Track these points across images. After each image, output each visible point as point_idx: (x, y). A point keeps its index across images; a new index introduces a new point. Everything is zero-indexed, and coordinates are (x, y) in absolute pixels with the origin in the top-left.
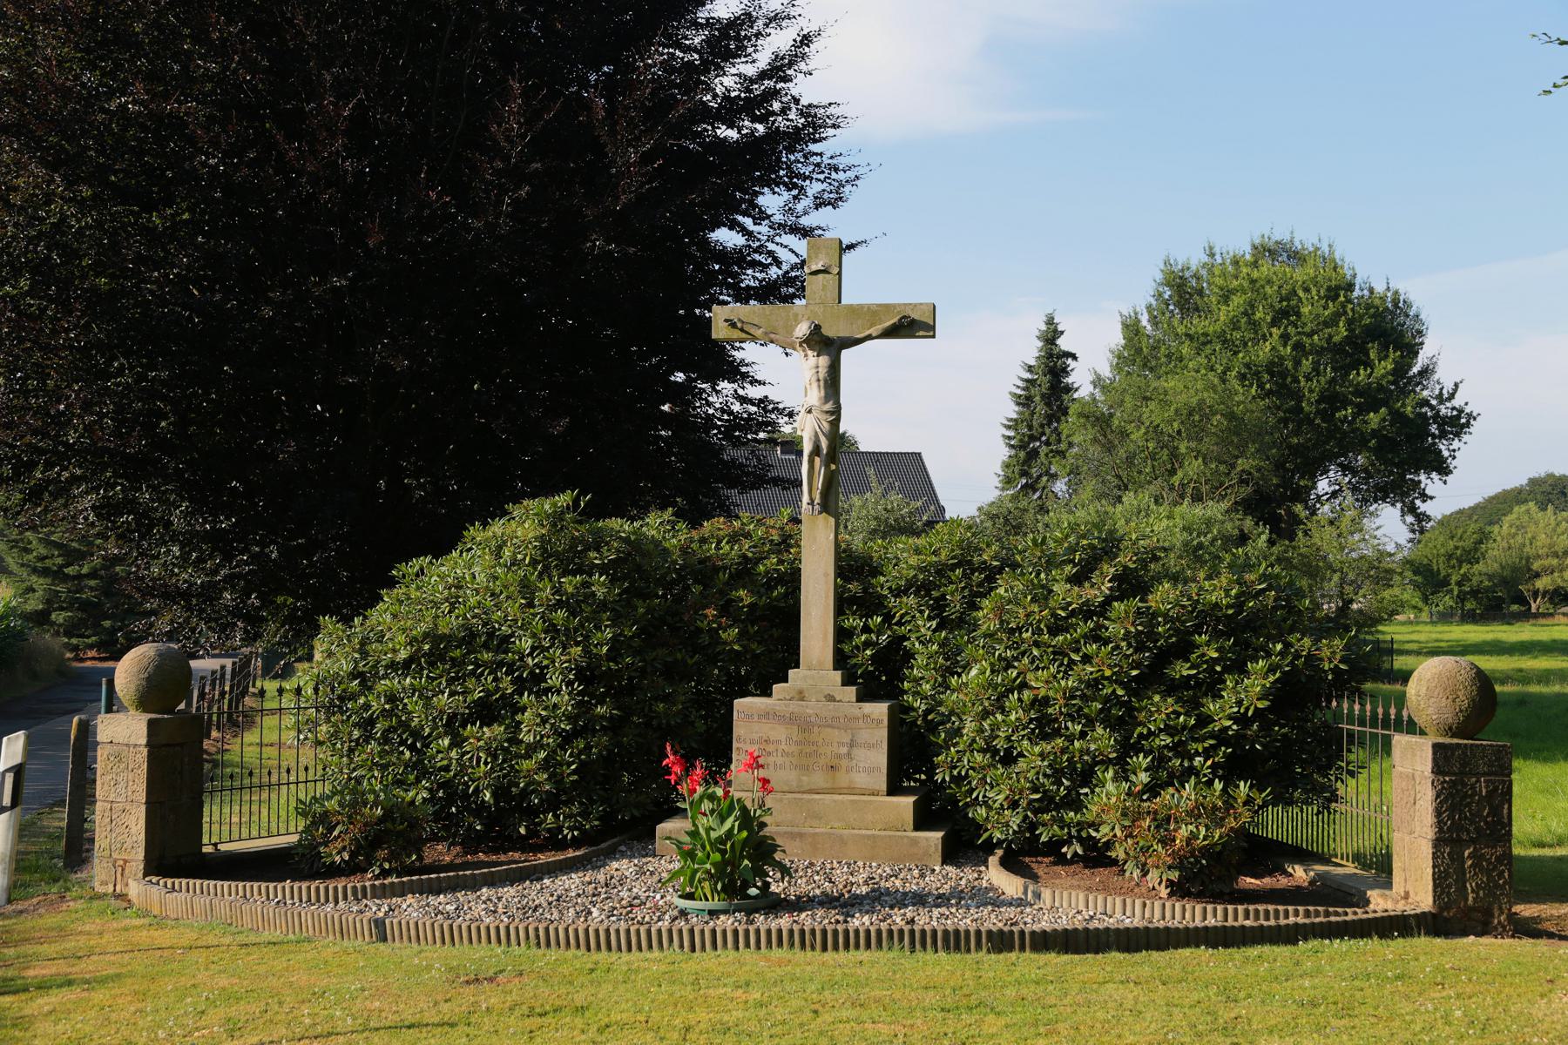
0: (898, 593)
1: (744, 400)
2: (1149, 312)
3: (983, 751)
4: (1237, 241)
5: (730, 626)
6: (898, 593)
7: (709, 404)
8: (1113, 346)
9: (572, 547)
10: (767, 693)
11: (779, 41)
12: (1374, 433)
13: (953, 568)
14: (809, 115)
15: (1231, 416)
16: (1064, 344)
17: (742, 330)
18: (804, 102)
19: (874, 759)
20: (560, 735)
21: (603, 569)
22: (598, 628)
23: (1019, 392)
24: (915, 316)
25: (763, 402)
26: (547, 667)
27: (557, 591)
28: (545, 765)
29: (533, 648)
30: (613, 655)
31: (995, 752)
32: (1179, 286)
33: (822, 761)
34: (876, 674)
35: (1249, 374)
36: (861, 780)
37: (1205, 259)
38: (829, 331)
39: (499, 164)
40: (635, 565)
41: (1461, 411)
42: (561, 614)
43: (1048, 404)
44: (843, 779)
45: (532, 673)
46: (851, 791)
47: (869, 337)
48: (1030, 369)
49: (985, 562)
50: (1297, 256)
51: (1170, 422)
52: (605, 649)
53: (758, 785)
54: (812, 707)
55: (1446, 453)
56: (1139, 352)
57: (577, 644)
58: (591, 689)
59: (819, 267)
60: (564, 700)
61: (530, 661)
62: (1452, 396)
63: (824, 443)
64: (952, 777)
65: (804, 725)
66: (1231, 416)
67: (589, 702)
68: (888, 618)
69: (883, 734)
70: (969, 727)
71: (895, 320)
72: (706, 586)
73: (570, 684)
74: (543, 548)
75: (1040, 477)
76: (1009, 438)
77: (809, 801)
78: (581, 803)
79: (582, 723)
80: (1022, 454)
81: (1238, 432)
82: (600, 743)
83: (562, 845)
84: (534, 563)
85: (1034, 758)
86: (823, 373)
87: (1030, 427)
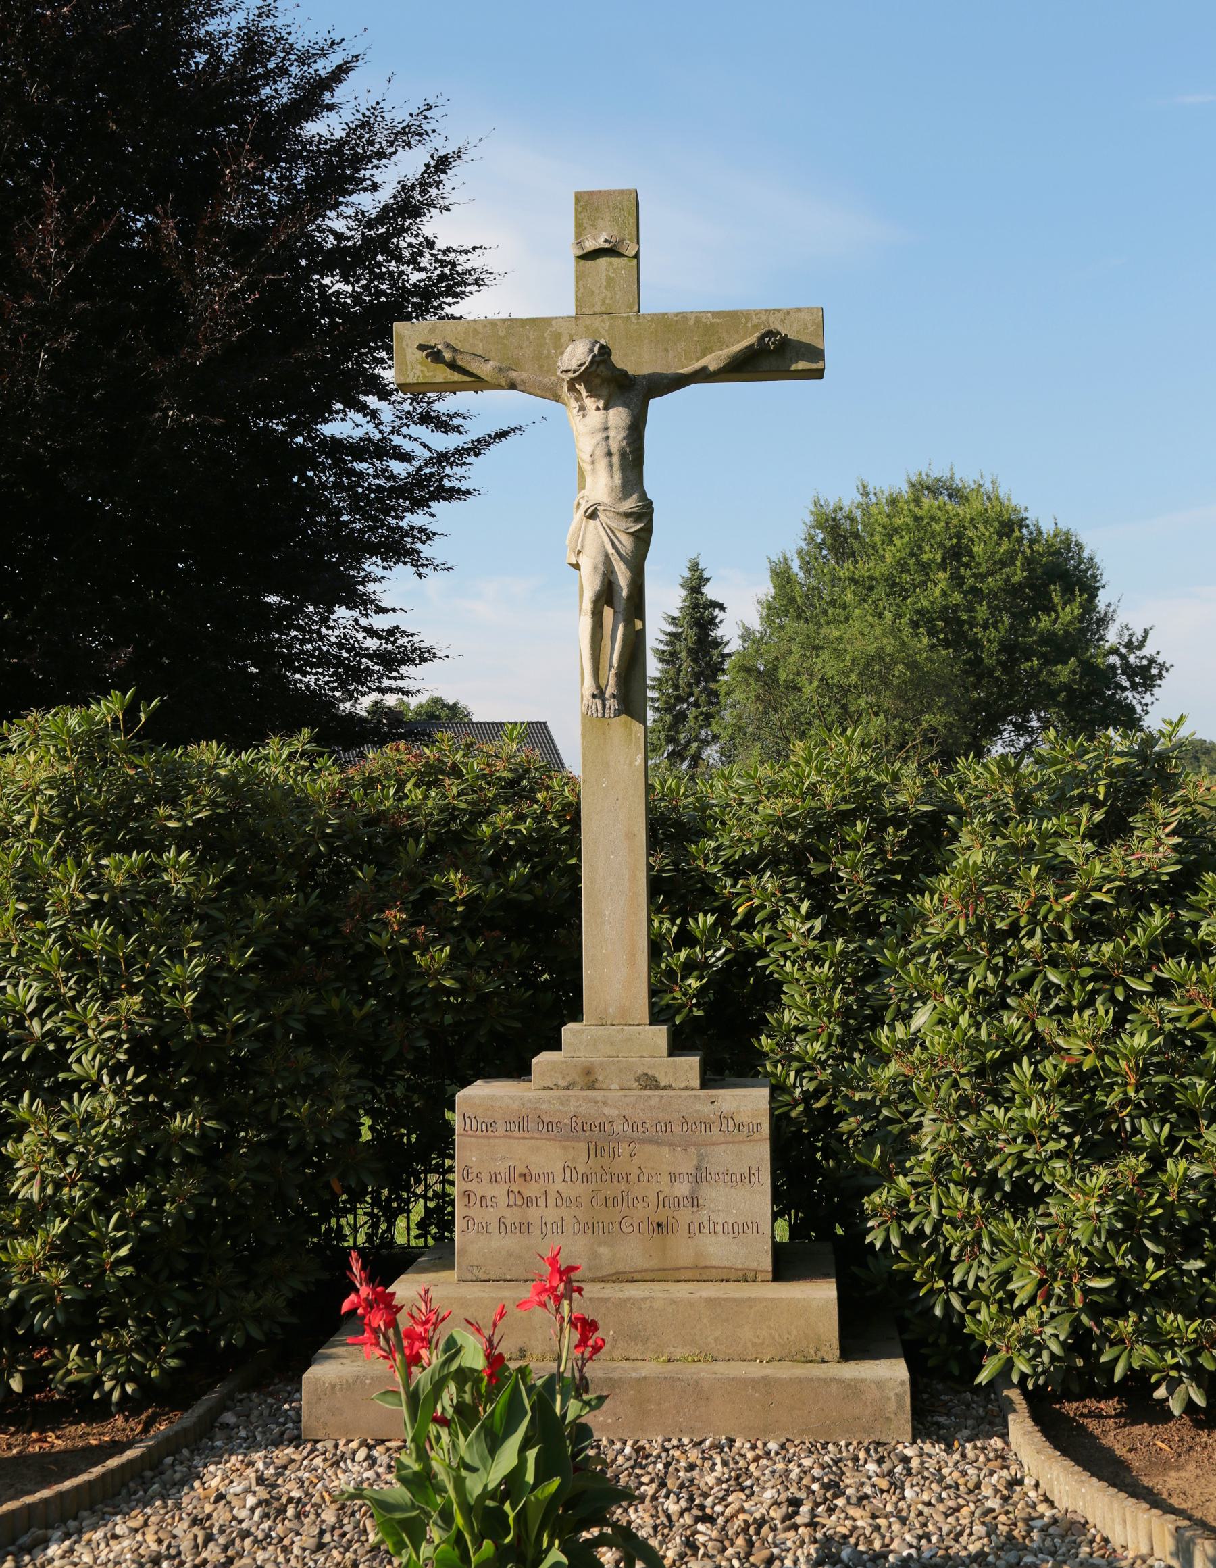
0: (740, 868)
1: (370, 632)
2: (801, 558)
3: (969, 1184)
4: (893, 480)
5: (434, 941)
6: (740, 868)
8: (762, 597)
9: (124, 798)
10: (521, 1071)
11: (408, 164)
12: (1067, 687)
13: (847, 818)
14: (443, 263)
15: (912, 665)
16: (711, 592)
17: (453, 366)
18: (441, 244)
19: (743, 1209)
20: (98, 1180)
21: (184, 839)
22: (175, 955)
23: (662, 647)
24: (791, 332)
25: (393, 632)
26: (71, 1038)
27: (92, 883)
28: (61, 1252)
29: (43, 1002)
30: (207, 1010)
31: (992, 1183)
32: (832, 528)
33: (639, 1213)
34: (720, 1026)
35: (923, 621)
36: (719, 1250)
37: (859, 498)
38: (636, 361)
39: (31, 302)
40: (240, 835)
41: (1152, 661)
42: (99, 929)
43: (695, 661)
44: (682, 1250)
45: (40, 1051)
46: (701, 1273)
47: (702, 376)
48: (674, 621)
49: (904, 807)
50: (956, 494)
51: (846, 673)
52: (190, 997)
53: (571, 1336)
54: (615, 1103)
55: (1138, 708)
56: (790, 601)
57: (133, 989)
58: (162, 1078)
59: (600, 243)
60: (105, 1107)
61: (35, 1025)
62: (1142, 645)
64: (904, 1237)
65: (599, 1140)
66: (912, 665)
67: (158, 1106)
68: (725, 912)
69: (761, 1153)
70: (932, 1133)
71: (752, 339)
72: (381, 867)
73: (118, 1070)
74: (65, 801)
75: (689, 742)
77: (621, 1303)
78: (142, 1322)
79: (143, 1157)
80: (668, 718)
81: (919, 688)
82: (180, 1195)
83: (100, 1412)
84: (46, 831)
85: (1084, 1202)
86: (617, 439)
87: (676, 687)
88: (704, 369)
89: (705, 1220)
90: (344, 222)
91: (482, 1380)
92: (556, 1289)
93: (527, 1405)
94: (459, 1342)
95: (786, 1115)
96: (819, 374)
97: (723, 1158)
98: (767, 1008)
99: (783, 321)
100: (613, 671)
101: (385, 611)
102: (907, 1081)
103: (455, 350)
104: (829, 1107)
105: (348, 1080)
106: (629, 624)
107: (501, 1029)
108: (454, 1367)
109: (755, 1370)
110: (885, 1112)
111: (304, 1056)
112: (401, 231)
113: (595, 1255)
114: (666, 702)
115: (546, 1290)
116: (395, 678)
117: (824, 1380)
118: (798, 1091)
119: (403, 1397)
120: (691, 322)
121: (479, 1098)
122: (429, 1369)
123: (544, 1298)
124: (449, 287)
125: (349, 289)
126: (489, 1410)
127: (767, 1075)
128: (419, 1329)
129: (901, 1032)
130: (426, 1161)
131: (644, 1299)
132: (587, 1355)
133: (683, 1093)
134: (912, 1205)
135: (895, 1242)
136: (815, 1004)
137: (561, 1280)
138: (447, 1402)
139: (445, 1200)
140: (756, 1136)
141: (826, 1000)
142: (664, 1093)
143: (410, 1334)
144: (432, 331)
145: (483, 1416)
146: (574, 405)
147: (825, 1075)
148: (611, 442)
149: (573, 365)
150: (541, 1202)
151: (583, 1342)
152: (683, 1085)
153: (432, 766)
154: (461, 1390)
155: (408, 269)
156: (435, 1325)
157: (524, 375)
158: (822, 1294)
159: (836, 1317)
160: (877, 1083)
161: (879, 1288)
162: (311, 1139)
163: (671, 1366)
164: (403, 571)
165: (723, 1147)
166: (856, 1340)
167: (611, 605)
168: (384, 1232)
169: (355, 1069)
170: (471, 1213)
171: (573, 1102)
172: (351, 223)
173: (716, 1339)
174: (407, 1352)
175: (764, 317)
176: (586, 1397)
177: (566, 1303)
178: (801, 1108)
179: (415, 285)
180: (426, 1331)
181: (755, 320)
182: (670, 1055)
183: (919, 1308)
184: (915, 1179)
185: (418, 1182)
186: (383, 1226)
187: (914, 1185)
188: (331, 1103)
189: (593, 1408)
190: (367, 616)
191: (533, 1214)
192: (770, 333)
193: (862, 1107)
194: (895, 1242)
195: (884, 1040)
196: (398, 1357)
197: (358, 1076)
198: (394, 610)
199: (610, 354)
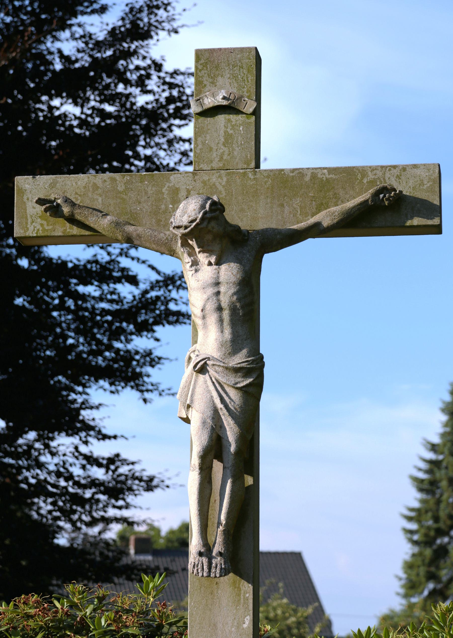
1: (91, 460)
7: (41, 466)
14: (172, 86)
17: (72, 220)
18: (168, 67)
23: (422, 475)
24: (406, 188)
25: (112, 461)
38: (246, 216)
48: (433, 448)
63: (231, 432)
71: (366, 196)
76: (411, 532)
80: (428, 552)
86: (228, 293)
87: (436, 519)
88: (317, 225)
90: (73, 44)
96: (437, 230)
99: (399, 177)
100: (221, 528)
101: (105, 437)
103: (73, 205)
106: (238, 480)
112: (128, 55)
114: (426, 535)
116: (120, 508)
120: (307, 178)
124: (177, 109)
125: (77, 111)
144: (53, 185)
146: (187, 259)
148: (222, 297)
149: (185, 220)
153: (60, 621)
155: (136, 91)
157: (140, 230)
164: (129, 395)
167: (220, 459)
172: (81, 45)
175: (379, 173)
179: (142, 108)
181: (371, 176)
190: (86, 443)
192: (384, 190)
198: (115, 437)
199: (222, 209)
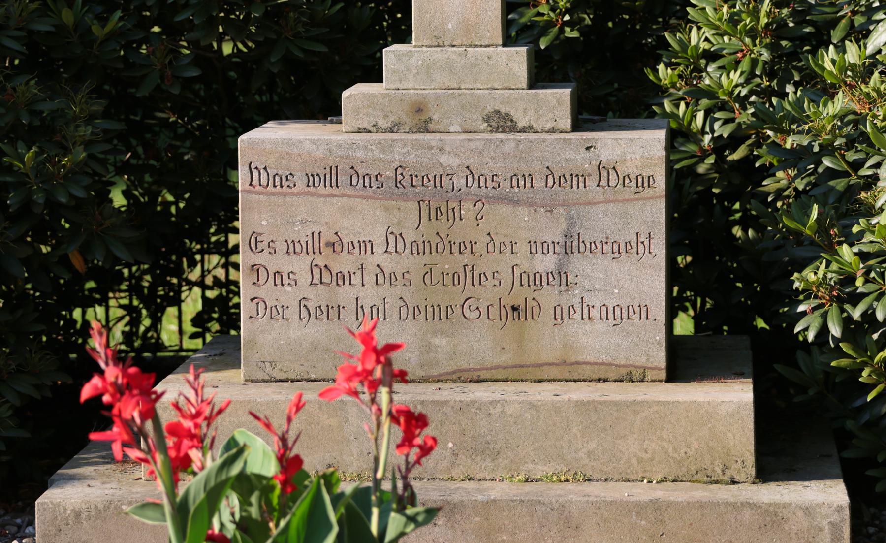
10: (329, 110)
19: (629, 283)
33: (487, 294)
36: (594, 341)
44: (545, 340)
46: (571, 372)
54: (454, 149)
64: (847, 322)
65: (435, 198)
69: (653, 215)
77: (463, 407)
89: (576, 301)
91: (272, 488)
92: (370, 372)
93: (333, 518)
94: (241, 441)
95: (690, 171)
97: (602, 220)
98: (667, 27)
102: (859, 120)
104: (749, 160)
105: (90, 119)
107: (300, 55)
108: (235, 470)
109: (641, 493)
110: (827, 162)
111: (28, 87)
113: (429, 348)
115: (358, 374)
117: (734, 505)
118: (707, 138)
119: (167, 509)
121: (268, 144)
122: (202, 475)
123: (356, 385)
126: (282, 523)
127: (665, 115)
128: (188, 424)
129: (853, 54)
130: (202, 238)
131: (493, 403)
132: (412, 458)
133: (547, 136)
134: (859, 282)
135: (835, 330)
136: (734, 20)
137: (378, 362)
138: (226, 517)
139: (230, 287)
140: (648, 192)
141: (749, 13)
142: (523, 136)
143: (175, 430)
145: (275, 532)
147: (745, 117)
150: (356, 279)
151: (407, 441)
152: (549, 126)
154: (245, 502)
156: (209, 420)
158: (731, 400)
159: (751, 425)
160: (817, 124)
161: (811, 392)
162: (39, 198)
163: (529, 487)
165: (601, 208)
166: (780, 451)
168: (148, 330)
169: (98, 107)
170: (261, 293)
171: (398, 148)
173: (590, 454)
174: (173, 454)
176: (410, 511)
177: (384, 391)
178: (711, 160)
180: (197, 426)
182: (532, 85)
183: (866, 417)
184: (865, 249)
185: (192, 264)
186: (147, 322)
187: (863, 256)
188: (66, 150)
189: (418, 525)
191: (345, 295)
193: (797, 158)
194: (835, 330)
195: (828, 65)
196: (159, 458)
197: (106, 115)
